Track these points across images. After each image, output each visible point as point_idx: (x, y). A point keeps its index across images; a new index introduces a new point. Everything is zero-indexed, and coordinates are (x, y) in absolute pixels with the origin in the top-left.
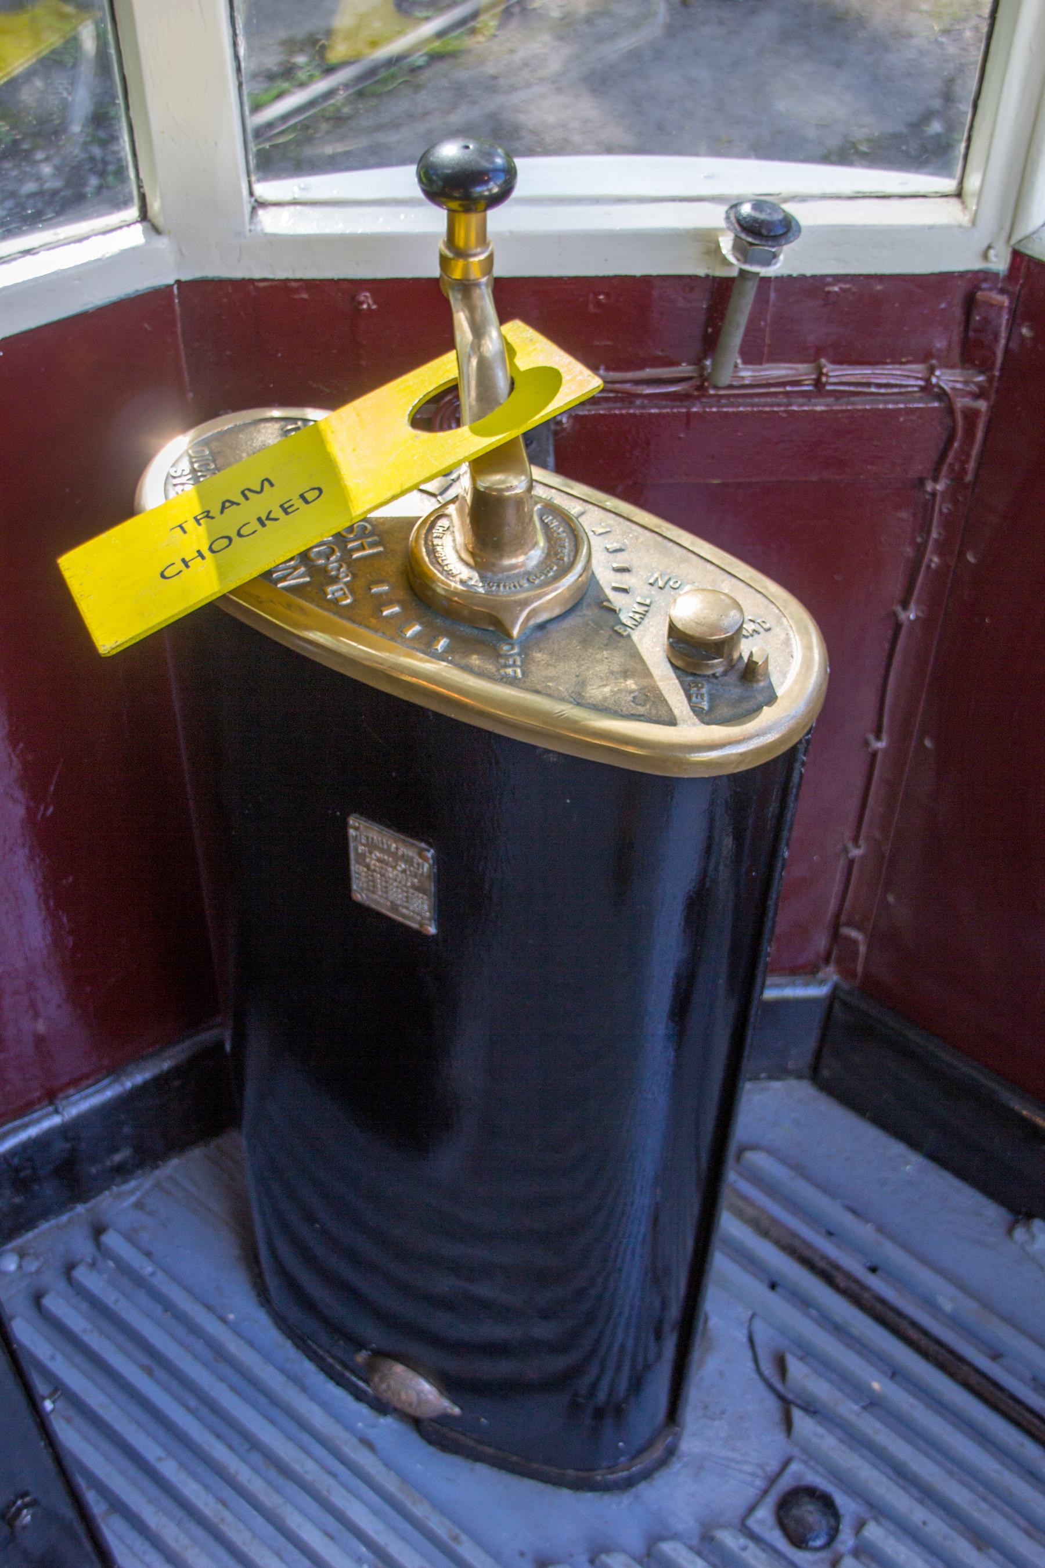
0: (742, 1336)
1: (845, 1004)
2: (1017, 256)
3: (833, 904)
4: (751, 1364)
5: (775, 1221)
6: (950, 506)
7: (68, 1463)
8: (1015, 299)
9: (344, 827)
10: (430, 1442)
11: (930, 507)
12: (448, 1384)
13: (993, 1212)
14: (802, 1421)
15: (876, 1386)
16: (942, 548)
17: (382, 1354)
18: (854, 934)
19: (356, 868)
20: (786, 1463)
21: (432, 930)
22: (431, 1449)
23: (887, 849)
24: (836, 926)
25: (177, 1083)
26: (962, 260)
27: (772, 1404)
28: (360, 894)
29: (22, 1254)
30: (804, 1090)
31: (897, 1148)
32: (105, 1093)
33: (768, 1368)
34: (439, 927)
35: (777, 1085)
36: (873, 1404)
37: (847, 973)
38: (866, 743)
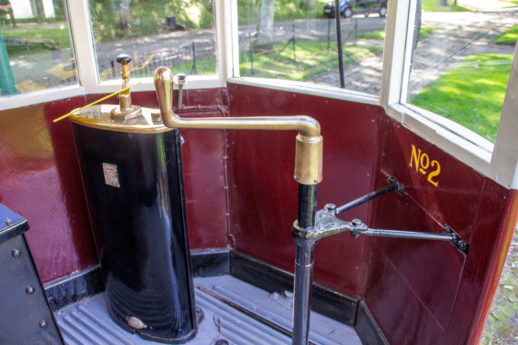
0: (212, 317)
1: (233, 253)
2: (228, 83)
3: (226, 231)
4: (213, 322)
5: (219, 296)
6: (165, 49)
7: (59, 328)
8: (228, 91)
9: (102, 166)
10: (143, 338)
11: (207, 113)
12: (144, 322)
13: (267, 293)
14: (222, 329)
15: (238, 322)
16: (228, 143)
17: (130, 316)
18: (231, 235)
19: (106, 176)
20: (219, 336)
21: (119, 186)
22: (143, 340)
23: (233, 214)
24: (228, 235)
25: (95, 274)
26: (219, 86)
27: (217, 327)
28: (107, 183)
29: (62, 312)
30: (230, 277)
31: (248, 285)
32: (81, 275)
33: (217, 322)
34: (120, 185)
35: (224, 277)
36: (239, 325)
37: (232, 246)
38: (224, 188)
